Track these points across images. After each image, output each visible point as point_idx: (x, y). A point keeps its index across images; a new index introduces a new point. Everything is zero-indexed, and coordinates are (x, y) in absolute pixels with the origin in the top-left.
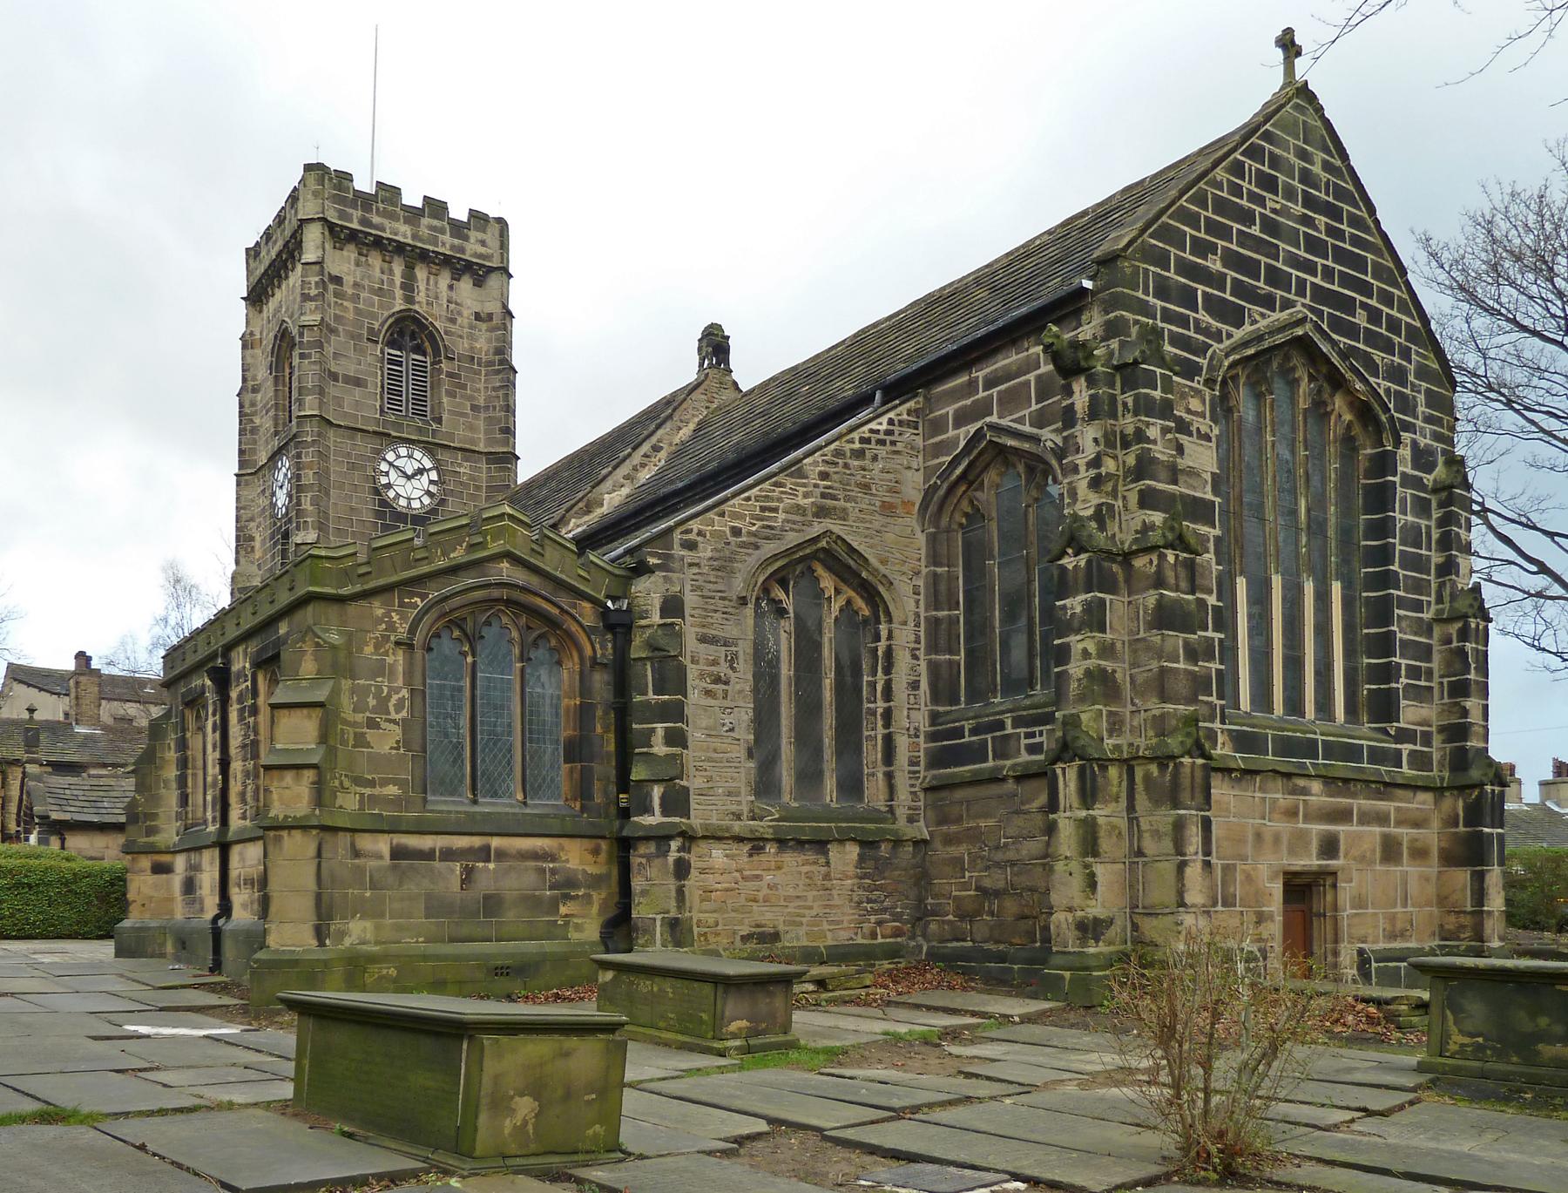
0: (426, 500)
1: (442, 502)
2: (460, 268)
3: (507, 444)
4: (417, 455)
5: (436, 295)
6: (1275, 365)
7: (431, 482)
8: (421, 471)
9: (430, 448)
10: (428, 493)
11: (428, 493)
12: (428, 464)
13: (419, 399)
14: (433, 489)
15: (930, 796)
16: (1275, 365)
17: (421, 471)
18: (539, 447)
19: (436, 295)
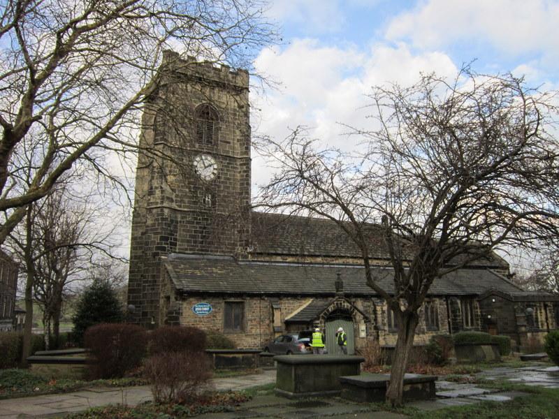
0: (212, 176)
1: (219, 177)
2: (222, 85)
3: (248, 154)
4: (209, 158)
5: (225, 100)
6: (523, 286)
7: (214, 169)
8: (210, 165)
9: (215, 156)
10: (213, 173)
11: (213, 173)
12: (213, 161)
13: (209, 137)
14: (215, 172)
15: (280, 365)
16: (523, 286)
17: (210, 165)
18: (33, 116)
19: (225, 100)
